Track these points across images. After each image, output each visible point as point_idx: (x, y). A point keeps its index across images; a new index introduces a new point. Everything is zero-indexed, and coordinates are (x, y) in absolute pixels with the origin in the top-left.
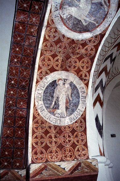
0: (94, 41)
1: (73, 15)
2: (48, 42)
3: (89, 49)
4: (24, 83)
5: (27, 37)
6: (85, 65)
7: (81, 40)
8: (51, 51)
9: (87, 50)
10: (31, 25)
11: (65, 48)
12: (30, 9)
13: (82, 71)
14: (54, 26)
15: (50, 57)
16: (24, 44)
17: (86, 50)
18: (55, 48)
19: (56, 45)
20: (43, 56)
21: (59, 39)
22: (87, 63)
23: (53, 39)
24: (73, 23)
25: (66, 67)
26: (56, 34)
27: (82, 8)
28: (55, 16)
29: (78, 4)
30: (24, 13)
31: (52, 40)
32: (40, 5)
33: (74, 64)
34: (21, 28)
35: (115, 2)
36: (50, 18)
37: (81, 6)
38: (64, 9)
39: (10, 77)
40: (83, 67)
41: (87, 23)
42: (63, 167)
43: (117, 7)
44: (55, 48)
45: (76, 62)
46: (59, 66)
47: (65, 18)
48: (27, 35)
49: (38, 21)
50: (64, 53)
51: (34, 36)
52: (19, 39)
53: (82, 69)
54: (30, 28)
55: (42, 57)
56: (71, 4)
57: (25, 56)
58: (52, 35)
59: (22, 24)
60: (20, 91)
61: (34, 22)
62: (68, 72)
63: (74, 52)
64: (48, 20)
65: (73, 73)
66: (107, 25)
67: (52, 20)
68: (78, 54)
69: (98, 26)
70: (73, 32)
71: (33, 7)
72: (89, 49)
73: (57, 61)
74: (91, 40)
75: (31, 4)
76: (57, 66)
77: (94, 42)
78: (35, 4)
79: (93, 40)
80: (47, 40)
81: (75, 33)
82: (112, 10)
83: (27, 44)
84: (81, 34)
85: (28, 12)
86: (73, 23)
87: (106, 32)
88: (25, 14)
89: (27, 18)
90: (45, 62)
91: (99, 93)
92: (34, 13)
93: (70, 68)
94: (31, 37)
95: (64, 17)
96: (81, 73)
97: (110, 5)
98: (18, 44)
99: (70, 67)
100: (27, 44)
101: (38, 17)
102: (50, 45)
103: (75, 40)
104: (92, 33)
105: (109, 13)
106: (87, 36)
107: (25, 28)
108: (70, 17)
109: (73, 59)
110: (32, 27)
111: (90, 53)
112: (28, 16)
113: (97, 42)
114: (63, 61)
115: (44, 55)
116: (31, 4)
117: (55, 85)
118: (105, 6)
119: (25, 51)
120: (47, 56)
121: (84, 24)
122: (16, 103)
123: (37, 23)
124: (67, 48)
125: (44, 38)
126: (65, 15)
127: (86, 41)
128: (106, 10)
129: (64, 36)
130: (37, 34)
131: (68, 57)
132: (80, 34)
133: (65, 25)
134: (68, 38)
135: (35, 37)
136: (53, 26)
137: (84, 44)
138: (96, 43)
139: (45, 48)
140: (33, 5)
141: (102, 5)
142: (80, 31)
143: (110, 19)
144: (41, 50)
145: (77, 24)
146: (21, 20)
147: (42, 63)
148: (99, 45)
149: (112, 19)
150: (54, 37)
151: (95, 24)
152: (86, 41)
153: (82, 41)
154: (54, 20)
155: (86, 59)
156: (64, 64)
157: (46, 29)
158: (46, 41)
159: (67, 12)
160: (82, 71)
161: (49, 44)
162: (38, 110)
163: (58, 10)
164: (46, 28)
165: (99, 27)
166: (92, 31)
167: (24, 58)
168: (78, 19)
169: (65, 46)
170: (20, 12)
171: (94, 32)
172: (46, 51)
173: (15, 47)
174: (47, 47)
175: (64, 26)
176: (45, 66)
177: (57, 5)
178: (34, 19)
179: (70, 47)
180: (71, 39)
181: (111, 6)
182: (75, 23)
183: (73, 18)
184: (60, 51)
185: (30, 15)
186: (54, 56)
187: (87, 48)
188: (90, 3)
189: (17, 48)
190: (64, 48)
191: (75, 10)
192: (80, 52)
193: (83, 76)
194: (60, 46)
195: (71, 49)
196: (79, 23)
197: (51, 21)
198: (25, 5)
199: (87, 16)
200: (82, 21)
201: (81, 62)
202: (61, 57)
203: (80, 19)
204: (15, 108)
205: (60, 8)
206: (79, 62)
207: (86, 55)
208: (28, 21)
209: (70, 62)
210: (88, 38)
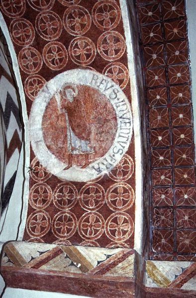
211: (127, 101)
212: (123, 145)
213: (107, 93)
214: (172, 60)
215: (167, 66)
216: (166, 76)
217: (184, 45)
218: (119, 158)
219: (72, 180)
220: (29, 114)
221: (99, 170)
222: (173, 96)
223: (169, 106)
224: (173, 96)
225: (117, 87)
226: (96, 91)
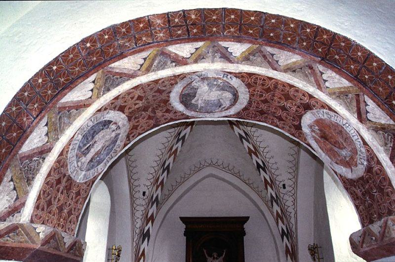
3: (165, 117)
4: (63, 79)
10: (152, 34)
12: (173, 27)
39: (60, 59)
42: (65, 241)
54: (147, 36)
56: (210, 85)
57: (102, 51)
60: (51, 86)
76: (130, 108)
91: (182, 218)
95: (194, 84)
100: (121, 42)
112: (162, 28)
114: (138, 109)
117: (106, 127)
119: (110, 46)
121: (193, 101)
122: (31, 100)
126: (195, 84)
141: (220, 107)
147: (125, 95)
155: (152, 122)
162: (71, 145)
167: (98, 53)
170: (164, 17)
173: (107, 33)
175: (182, 88)
182: (191, 94)
204: (23, 106)
211: (336, 114)
212: (358, 140)
213: (326, 116)
214: (346, 50)
215: (348, 55)
216: (355, 61)
217: (339, 38)
218: (363, 150)
219: (36, 201)
220: (315, 151)
221: (362, 164)
222: (372, 68)
223: (377, 77)
224: (372, 68)
225: (325, 110)
226: (321, 119)
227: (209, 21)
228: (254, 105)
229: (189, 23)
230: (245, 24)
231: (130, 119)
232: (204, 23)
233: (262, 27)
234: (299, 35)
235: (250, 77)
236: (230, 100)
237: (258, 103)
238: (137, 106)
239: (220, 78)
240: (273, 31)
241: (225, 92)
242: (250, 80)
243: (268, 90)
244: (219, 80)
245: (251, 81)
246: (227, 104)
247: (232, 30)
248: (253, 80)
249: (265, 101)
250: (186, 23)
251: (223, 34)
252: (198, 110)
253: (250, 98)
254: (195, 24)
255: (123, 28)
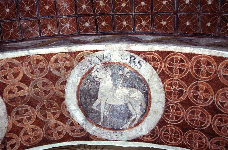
0: (75, 129)
1: (101, 85)
2: (46, 63)
3: (59, 129)
5: (35, 22)
6: (31, 136)
7: (67, 111)
8: (32, 73)
9: (56, 127)
10: (58, 23)
11: (46, 92)
12: (80, 15)
13: (19, 136)
14: (75, 63)
15: (21, 75)
16: (20, 19)
17: (56, 125)
18: (39, 78)
19: (45, 77)
20: (18, 62)
21: (57, 78)
22: (36, 137)
23: (54, 67)
24: (90, 89)
25: (13, 108)
26: (63, 71)
27: (115, 94)
28: (90, 61)
29: (119, 87)
30: (71, 7)
31: (51, 67)
32: (92, 28)
33: (24, 118)
34: (47, 7)
35: (139, 133)
36: (84, 53)
37: (118, 91)
38: (104, 69)
40: (26, 134)
41: (97, 109)
43: (133, 138)
44: (39, 78)
45: (29, 119)
46: (12, 96)
47: (93, 75)
48: (39, 21)
49: (68, 32)
50: (37, 94)
51: (40, 32)
52: (28, 8)
53: (21, 134)
54: (52, 23)
55: (15, 61)
56: (114, 76)
58: (60, 64)
59: (53, 8)
61: (64, 26)
62: (6, 114)
63: (46, 109)
64: (81, 52)
65: (9, 123)
66: (104, 137)
67: (83, 58)
68: (45, 116)
69: (99, 126)
70: (75, 94)
71: (85, 19)
72: (59, 129)
73: (20, 89)
74: (74, 126)
75: (89, 15)
76: (11, 92)
77: (73, 131)
78: (90, 21)
79: (75, 127)
80: (49, 60)
81: (76, 97)
82: (127, 133)
83: (24, 24)
84: (78, 107)
85: (76, 13)
86: (90, 89)
87: (94, 140)
88: (71, 10)
89: (66, 13)
90: (8, 69)
92: (77, 23)
93: (15, 115)
94: (38, 28)
95: (94, 74)
96: (15, 136)
97: (133, 128)
98: (17, 8)
99: (17, 113)
100: (24, 24)
101: (73, 30)
102: (43, 67)
103: (64, 102)
104: (84, 122)
105: (122, 131)
106: (78, 116)
107: (49, 15)
108: (97, 81)
109: (33, 112)
110: (54, 25)
111: (52, 133)
112: (69, 16)
113: (75, 134)
114: (22, 97)
115: (22, 63)
116: (89, 15)
118: (129, 123)
120: (21, 69)
121: (94, 106)
123: (63, 31)
124: (47, 96)
125: (50, 54)
126: (96, 73)
127: (70, 118)
128: (125, 126)
129: (65, 83)
130: (46, 36)
131: (32, 103)
132: (77, 106)
133: (83, 78)
134: (63, 91)
135: (40, 35)
136: (74, 62)
137: (64, 118)
138: (73, 133)
139: (33, 61)
140: (88, 18)
142: (82, 104)
143: (114, 137)
144: (27, 56)
145: (91, 95)
146: (59, 5)
147: (5, 65)
148: (71, 141)
149: (116, 139)
150: (58, 69)
151: (100, 121)
152: (70, 118)
153: (67, 113)
154: (84, 60)
155: (41, 132)
156: (19, 101)
157: (65, 53)
158: (46, 58)
159: (103, 75)
160: (19, 136)
161: (42, 64)
163: (101, 61)
164: (67, 51)
165: (98, 128)
166: (90, 121)
168: (97, 94)
169: (49, 91)
171: (88, 124)
172: (30, 63)
173: (10, 5)
174: (37, 63)
175: (80, 78)
176: (2, 73)
177: (107, 57)
178: (68, 25)
179: (50, 99)
180: (64, 95)
181: (131, 130)
182: (91, 92)
183: (97, 86)
184: (38, 87)
185: (72, 17)
186: (26, 80)
187: (59, 125)
188: (127, 102)
189: (10, 9)
190: (45, 91)
191: (110, 86)
192: (48, 118)
193: (10, 143)
194: (47, 84)
195: (48, 101)
196: (93, 98)
197: (81, 56)
198: (84, 6)
199: (107, 105)
200: (98, 100)
201: (34, 126)
202: (28, 91)
203: (98, 96)
205: (104, 63)
206: (32, 124)
207: (48, 129)
208: (61, 16)
209: (26, 111)
210: (75, 120)
227: (118, 10)
228: (173, 112)
229: (97, 12)
230: (157, 13)
231: (9, 111)
232: (113, 14)
233: (176, 13)
234: (220, 14)
235: (163, 58)
236: (141, 105)
237: (178, 109)
238: (20, 93)
239: (125, 65)
240: (188, 17)
241: (134, 89)
242: (163, 64)
243: (188, 79)
244: (125, 69)
245: (165, 67)
246: (137, 112)
247: (144, 23)
248: (179, 139)
249: (187, 104)
250: (94, 12)
251: (134, 29)
252: (100, 123)
253: (167, 101)
254: (103, 14)
255: (27, 5)
